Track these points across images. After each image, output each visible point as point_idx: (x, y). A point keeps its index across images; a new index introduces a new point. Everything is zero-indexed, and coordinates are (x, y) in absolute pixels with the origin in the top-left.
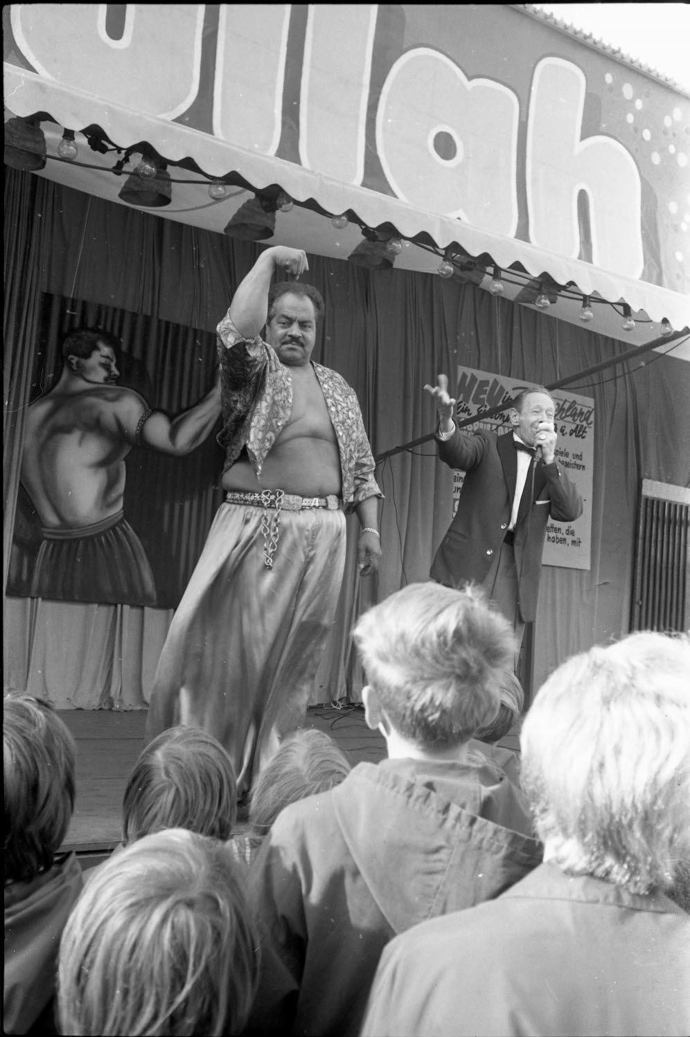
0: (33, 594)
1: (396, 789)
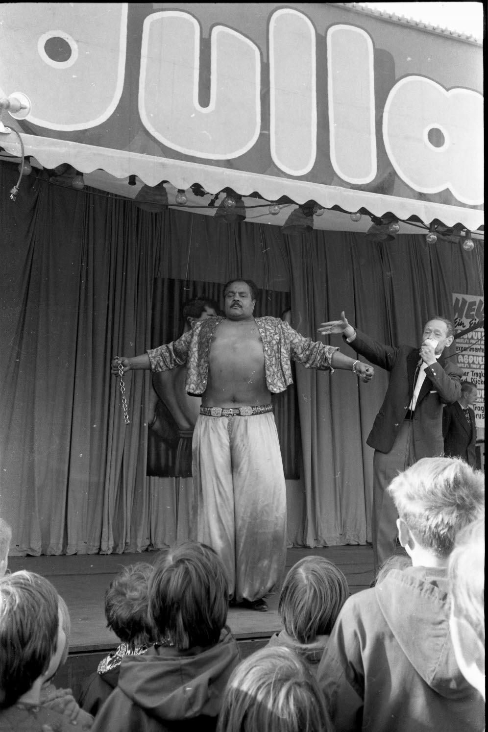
0: (177, 474)
1: (413, 585)
